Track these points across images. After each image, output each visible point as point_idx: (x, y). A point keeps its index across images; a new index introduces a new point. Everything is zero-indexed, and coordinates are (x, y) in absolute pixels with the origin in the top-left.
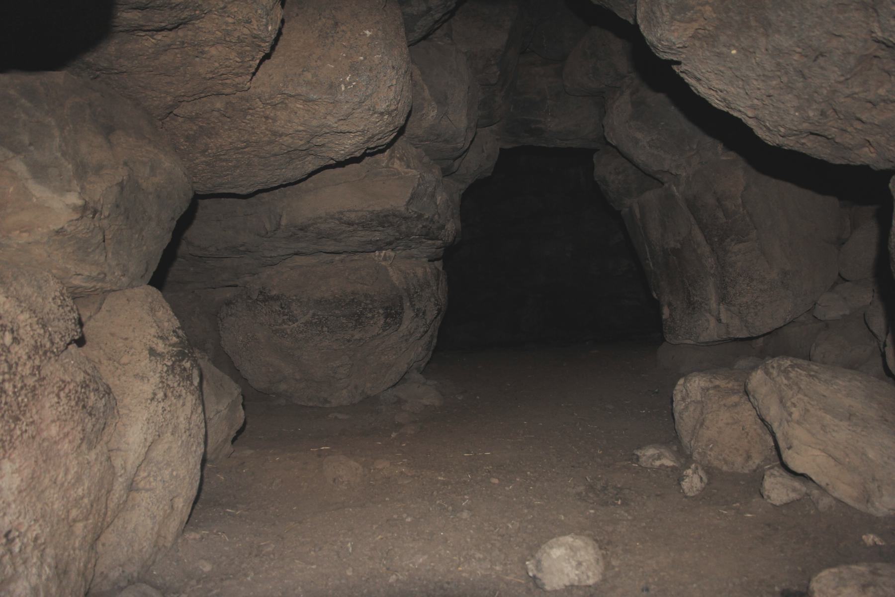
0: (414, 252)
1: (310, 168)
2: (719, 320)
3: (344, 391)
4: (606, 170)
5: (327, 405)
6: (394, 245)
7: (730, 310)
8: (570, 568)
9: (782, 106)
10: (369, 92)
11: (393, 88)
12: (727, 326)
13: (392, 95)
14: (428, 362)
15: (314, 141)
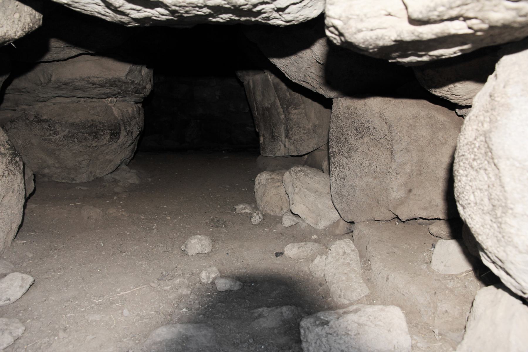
2: (285, 146)
3: (84, 175)
5: (74, 182)
12: (288, 149)
14: (132, 159)
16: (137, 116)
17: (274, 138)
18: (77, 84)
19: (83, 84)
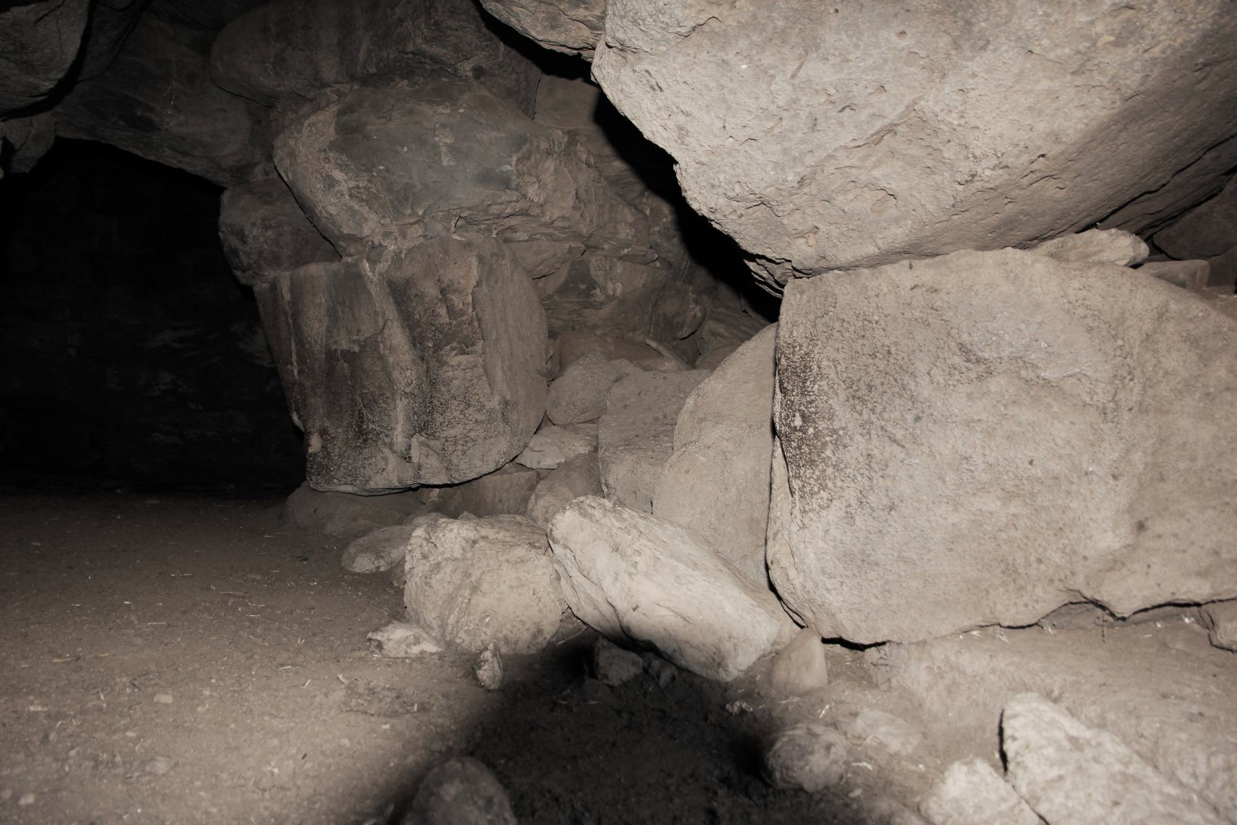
4: (244, 221)
7: (428, 446)
8: (476, 813)
17: (363, 436)
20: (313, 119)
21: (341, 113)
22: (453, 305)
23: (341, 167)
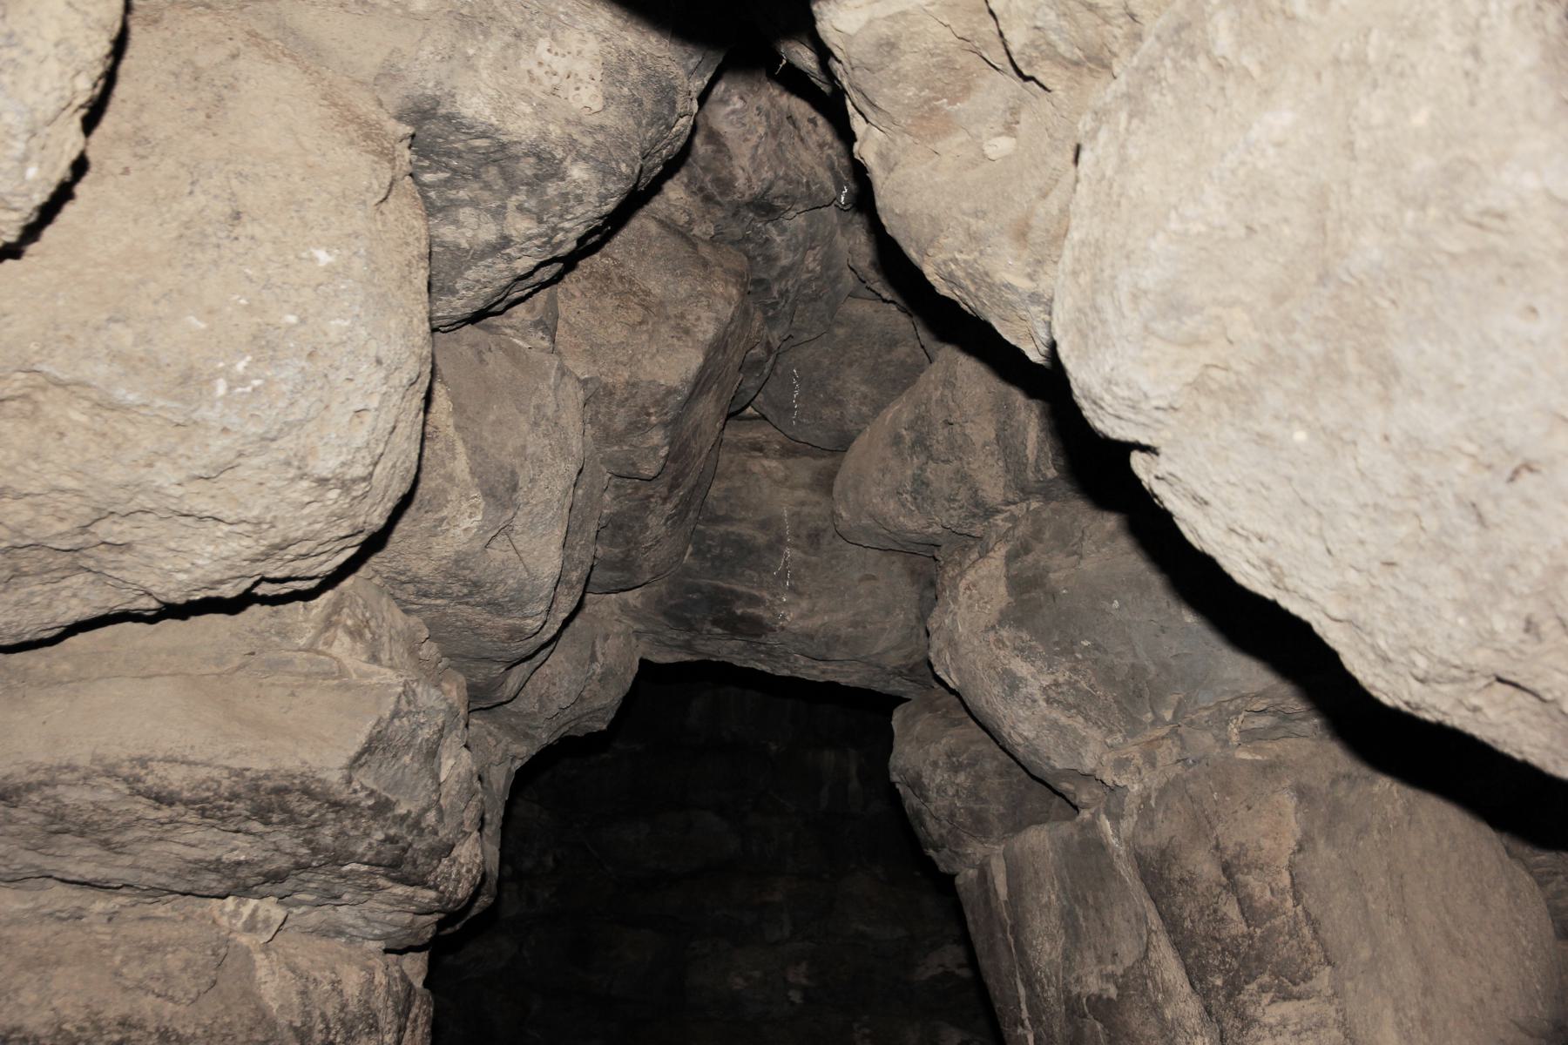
0: (346, 915)
1: (77, 611)
4: (922, 755)
6: (288, 885)
9: (1418, 593)
10: (297, 414)
11: (368, 418)
13: (361, 436)
15: (104, 530)
16: (387, 1019)
18: (73, 796)
19: (105, 795)
20: (971, 576)
21: (1011, 558)
22: (1250, 897)
23: (1023, 651)
